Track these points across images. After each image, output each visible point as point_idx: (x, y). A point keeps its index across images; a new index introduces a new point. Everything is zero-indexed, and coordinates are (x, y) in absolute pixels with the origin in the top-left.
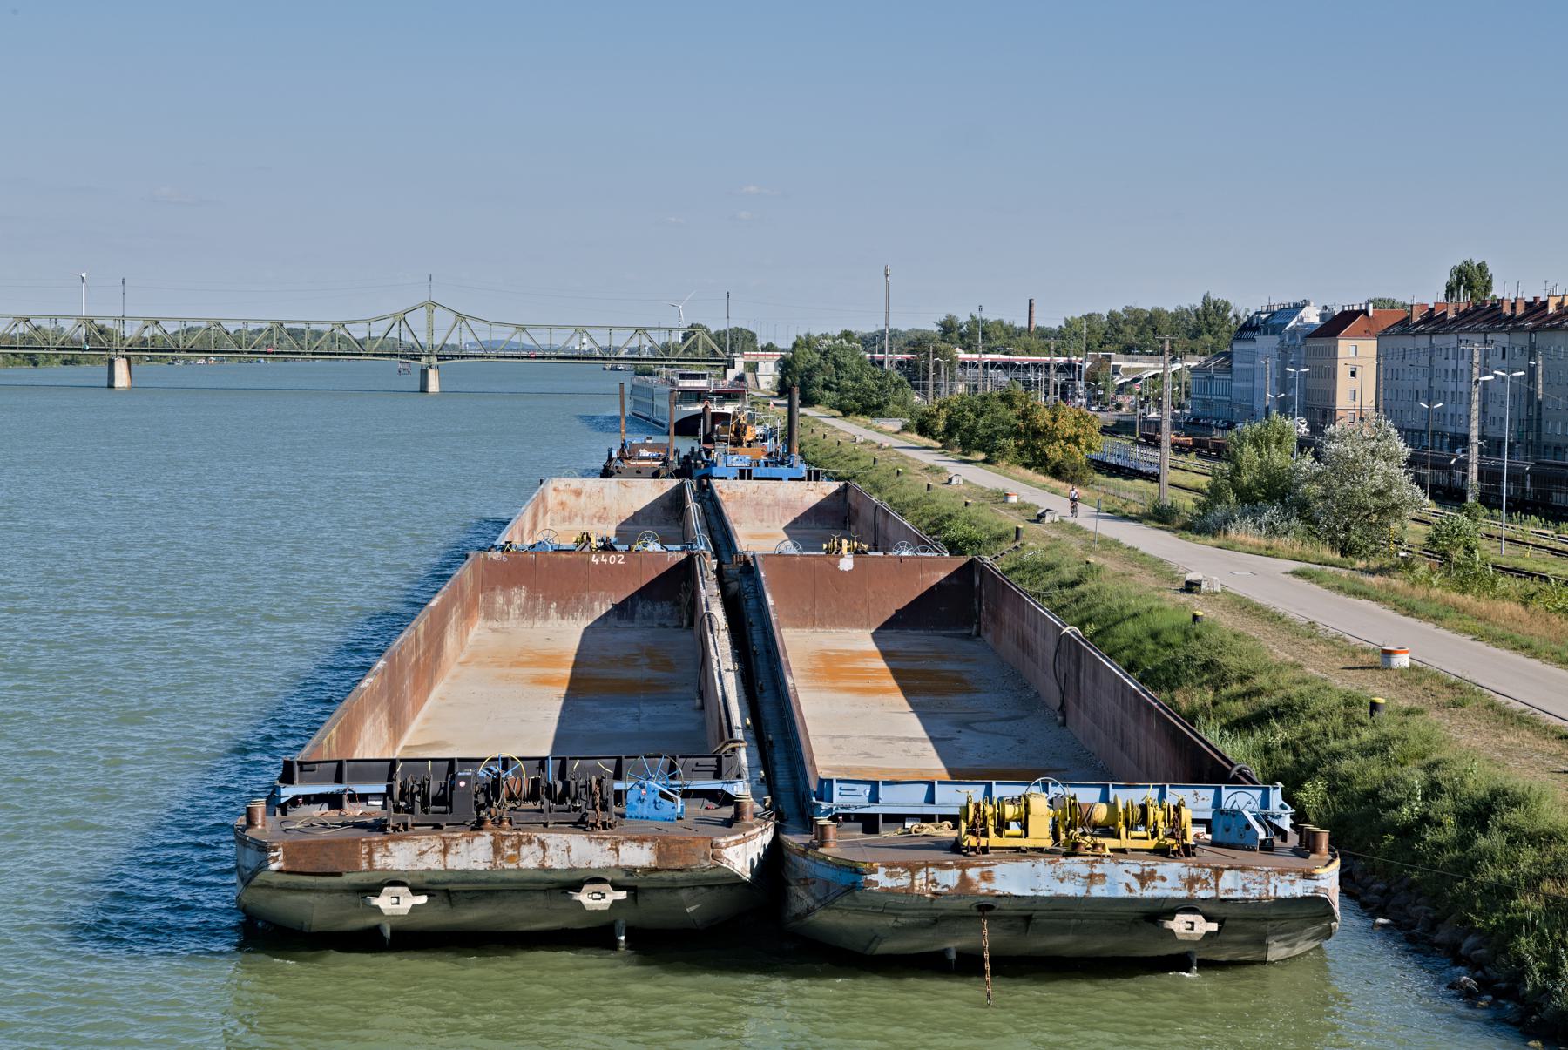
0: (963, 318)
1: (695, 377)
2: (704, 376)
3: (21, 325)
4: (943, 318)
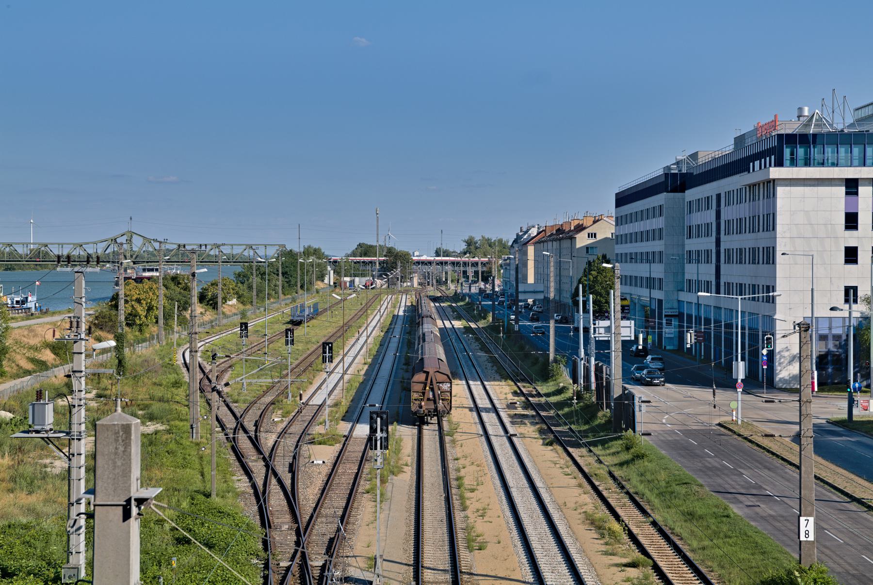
0: (477, 238)
1: (152, 270)
2: (157, 270)
3: (78, 249)
4: (466, 239)
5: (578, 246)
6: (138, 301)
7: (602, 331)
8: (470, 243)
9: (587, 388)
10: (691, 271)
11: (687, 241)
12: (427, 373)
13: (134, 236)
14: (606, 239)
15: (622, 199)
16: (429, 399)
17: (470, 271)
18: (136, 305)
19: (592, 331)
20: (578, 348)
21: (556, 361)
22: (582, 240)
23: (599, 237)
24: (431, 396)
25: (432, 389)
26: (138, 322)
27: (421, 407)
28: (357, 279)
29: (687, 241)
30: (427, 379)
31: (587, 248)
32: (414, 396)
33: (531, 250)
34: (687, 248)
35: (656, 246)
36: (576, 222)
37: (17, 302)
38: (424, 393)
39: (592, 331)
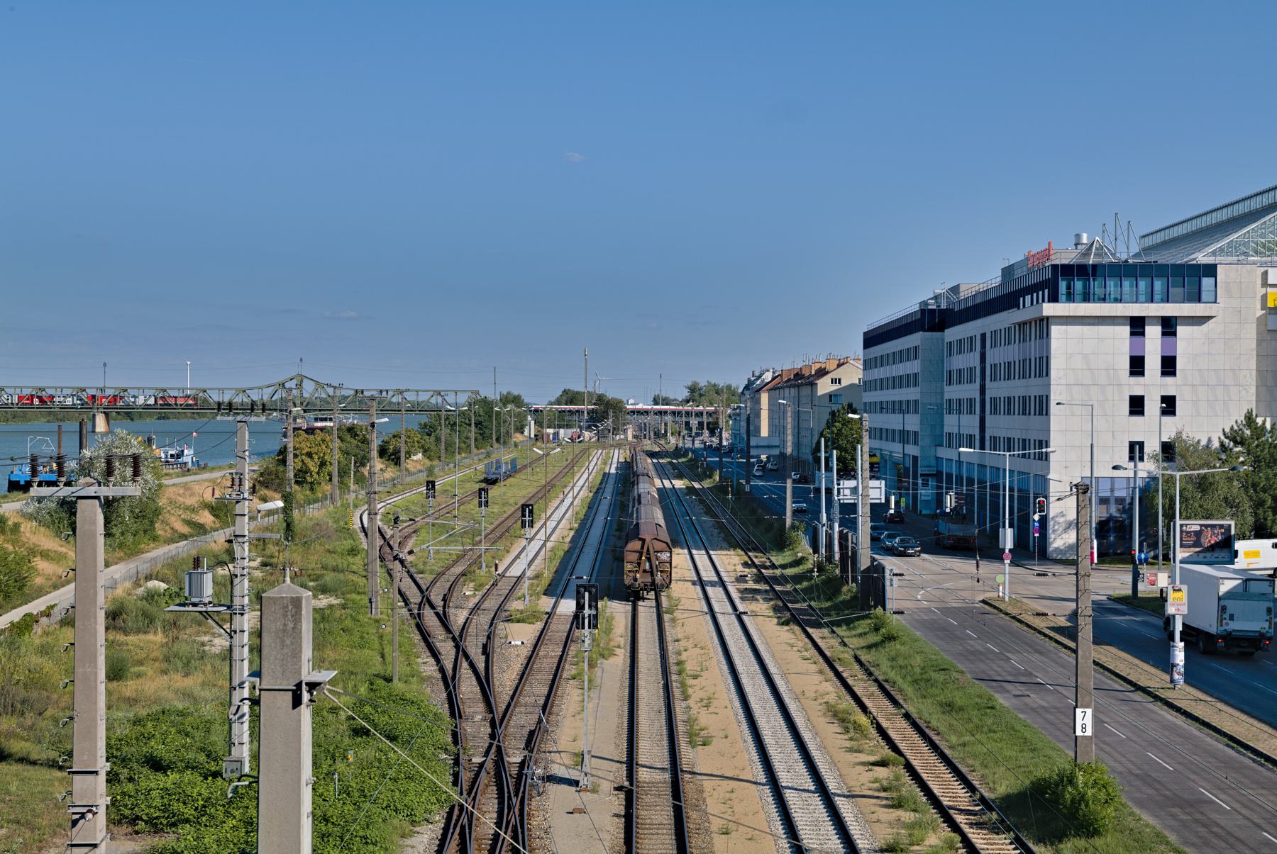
0: (702, 383)
1: (325, 420)
5: (820, 392)
6: (310, 455)
7: (847, 492)
8: (693, 389)
9: (830, 558)
10: (951, 423)
11: (947, 389)
12: (643, 540)
13: (305, 381)
14: (852, 385)
15: (872, 339)
16: (645, 571)
17: (694, 422)
18: (307, 460)
19: (836, 492)
20: (820, 512)
21: (793, 527)
22: (824, 387)
23: (844, 383)
24: (648, 567)
25: (649, 559)
26: (309, 479)
27: (636, 580)
28: (562, 431)
29: (947, 389)
30: (642, 547)
31: (831, 396)
32: (628, 567)
33: (764, 398)
34: (947, 397)
35: (911, 394)
36: (818, 366)
37: (172, 456)
38: (639, 564)
39: (836, 492)
